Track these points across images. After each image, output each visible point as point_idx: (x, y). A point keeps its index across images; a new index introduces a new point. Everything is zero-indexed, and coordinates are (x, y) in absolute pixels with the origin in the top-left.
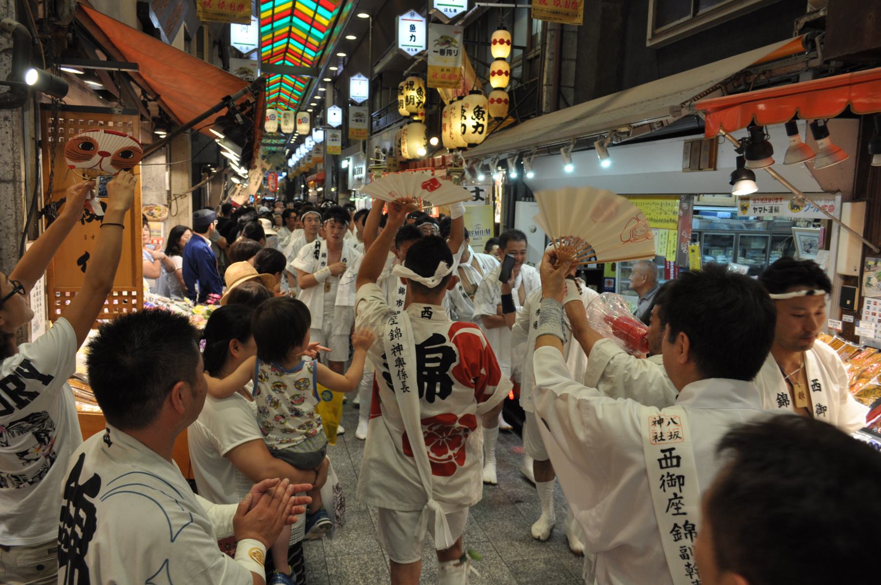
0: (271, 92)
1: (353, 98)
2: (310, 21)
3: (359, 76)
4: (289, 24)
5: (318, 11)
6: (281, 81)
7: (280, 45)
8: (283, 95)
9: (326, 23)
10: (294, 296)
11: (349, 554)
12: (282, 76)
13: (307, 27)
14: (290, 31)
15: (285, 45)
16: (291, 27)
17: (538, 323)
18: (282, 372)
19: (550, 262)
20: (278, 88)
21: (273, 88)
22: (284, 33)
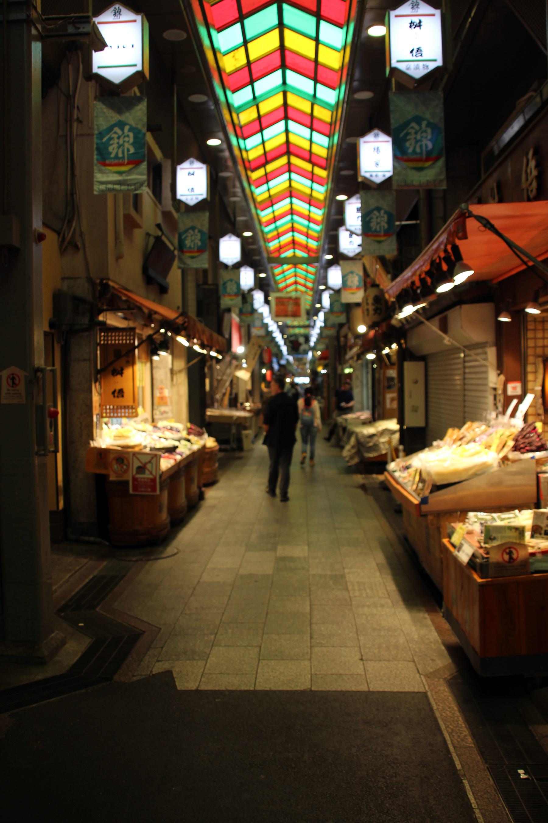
0: (280, 230)
1: (367, 175)
2: (310, 176)
3: (376, 136)
4: (282, 89)
5: (314, 139)
6: (292, 212)
7: (286, 238)
8: (299, 280)
9: (321, 197)
10: (405, 182)
11: (459, 736)
12: (289, 159)
13: (306, 222)
14: (285, 104)
15: (287, 184)
16: (285, 93)
17: (465, 439)
18: (90, 16)
19: (268, 492)
20: (289, 226)
21: (282, 225)
22: (282, 167)
